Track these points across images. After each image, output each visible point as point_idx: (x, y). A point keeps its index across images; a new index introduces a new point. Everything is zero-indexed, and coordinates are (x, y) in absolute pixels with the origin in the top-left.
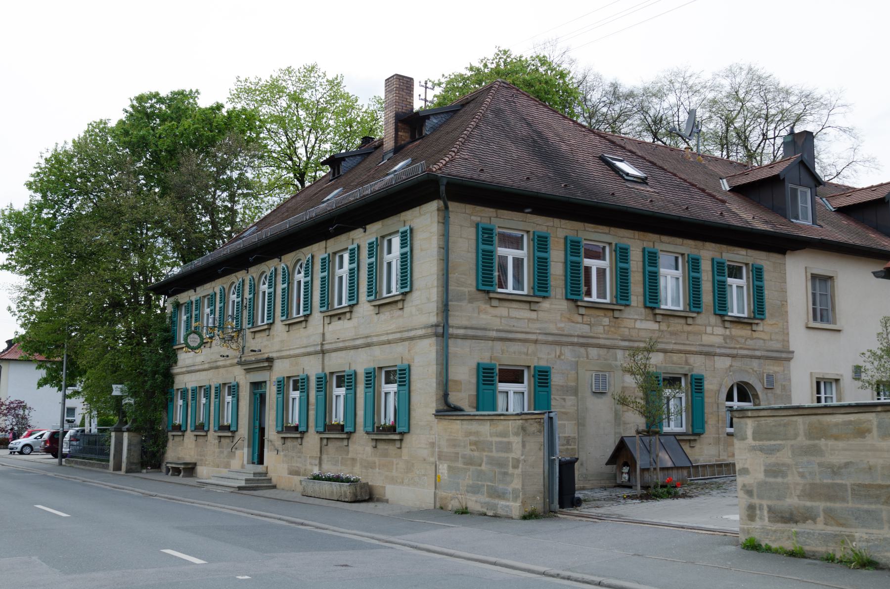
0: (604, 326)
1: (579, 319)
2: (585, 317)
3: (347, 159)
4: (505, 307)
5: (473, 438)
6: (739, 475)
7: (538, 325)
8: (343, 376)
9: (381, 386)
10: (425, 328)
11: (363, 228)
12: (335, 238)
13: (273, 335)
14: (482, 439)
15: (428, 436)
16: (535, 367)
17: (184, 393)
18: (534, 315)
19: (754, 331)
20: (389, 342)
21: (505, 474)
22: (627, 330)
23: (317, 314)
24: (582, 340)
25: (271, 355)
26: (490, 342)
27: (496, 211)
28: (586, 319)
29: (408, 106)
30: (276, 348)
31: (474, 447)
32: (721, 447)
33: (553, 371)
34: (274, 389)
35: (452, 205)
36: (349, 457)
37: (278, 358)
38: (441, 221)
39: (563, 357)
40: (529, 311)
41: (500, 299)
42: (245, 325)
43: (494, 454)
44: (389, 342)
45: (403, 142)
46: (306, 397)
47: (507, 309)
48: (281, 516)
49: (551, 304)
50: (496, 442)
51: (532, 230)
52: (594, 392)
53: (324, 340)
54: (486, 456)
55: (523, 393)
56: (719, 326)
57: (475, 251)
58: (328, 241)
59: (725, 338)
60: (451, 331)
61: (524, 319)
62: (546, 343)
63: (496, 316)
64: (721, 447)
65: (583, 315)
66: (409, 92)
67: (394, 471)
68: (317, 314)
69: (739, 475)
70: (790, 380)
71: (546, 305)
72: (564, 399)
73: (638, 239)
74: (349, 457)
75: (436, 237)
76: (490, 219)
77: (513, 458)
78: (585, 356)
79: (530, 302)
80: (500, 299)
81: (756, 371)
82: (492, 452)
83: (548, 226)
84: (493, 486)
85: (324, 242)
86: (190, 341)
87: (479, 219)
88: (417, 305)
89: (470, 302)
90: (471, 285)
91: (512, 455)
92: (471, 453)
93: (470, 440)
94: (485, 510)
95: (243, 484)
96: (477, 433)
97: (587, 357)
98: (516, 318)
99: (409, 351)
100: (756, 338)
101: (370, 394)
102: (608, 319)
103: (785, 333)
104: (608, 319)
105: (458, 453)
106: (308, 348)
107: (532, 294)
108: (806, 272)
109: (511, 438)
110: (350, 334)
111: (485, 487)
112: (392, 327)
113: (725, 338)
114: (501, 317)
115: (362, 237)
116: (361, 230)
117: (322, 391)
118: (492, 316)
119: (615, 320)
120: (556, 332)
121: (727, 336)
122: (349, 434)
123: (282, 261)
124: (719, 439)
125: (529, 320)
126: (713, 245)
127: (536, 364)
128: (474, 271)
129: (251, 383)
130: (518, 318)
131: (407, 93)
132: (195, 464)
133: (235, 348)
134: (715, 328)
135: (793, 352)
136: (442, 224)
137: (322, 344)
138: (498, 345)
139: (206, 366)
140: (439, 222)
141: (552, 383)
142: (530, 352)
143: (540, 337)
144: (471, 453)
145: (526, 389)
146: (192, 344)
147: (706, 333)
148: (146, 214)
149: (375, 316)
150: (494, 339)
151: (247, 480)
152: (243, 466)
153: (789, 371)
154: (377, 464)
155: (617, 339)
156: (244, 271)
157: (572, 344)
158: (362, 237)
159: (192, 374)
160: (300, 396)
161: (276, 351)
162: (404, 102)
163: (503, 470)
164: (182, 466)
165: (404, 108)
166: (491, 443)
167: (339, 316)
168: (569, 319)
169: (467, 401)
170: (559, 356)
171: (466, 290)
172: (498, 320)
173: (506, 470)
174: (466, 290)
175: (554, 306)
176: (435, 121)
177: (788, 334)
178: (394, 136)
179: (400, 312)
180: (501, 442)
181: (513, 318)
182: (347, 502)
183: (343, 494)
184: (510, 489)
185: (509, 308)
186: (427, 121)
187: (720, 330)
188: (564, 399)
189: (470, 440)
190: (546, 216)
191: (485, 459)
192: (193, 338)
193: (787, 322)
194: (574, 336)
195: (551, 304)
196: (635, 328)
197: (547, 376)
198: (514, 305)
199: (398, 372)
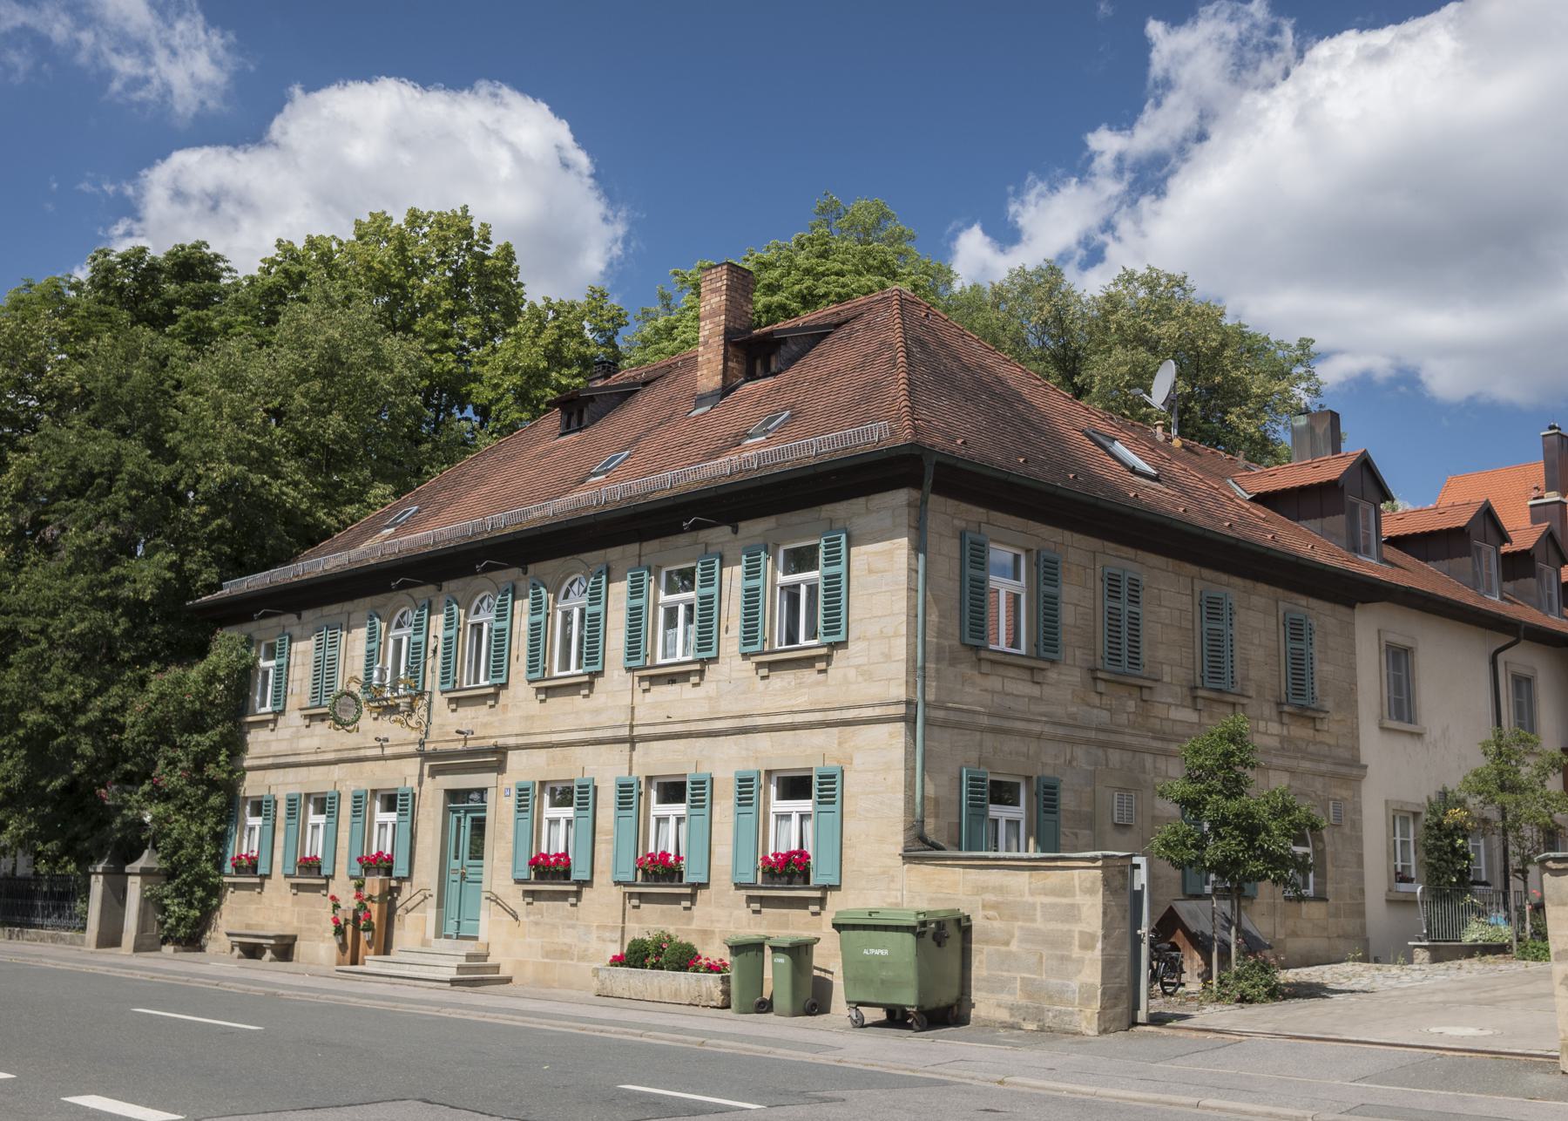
0: (1129, 713)
1: (1096, 700)
2: (1104, 697)
3: (597, 400)
4: (999, 675)
5: (990, 897)
6: (1556, 960)
7: (1043, 708)
12: (662, 540)
13: (505, 706)
14: (1010, 898)
15: (884, 892)
16: (1039, 778)
17: (258, 808)
18: (1035, 691)
19: (1317, 730)
20: (794, 727)
21: (1063, 959)
22: (1157, 721)
23: (616, 673)
24: (1102, 736)
25: (501, 742)
26: (978, 733)
28: (1105, 700)
31: (991, 913)
32: (1278, 920)
33: (1063, 786)
34: (510, 802)
35: (933, 498)
36: (693, 927)
37: (518, 747)
38: (913, 525)
39: (1074, 764)
40: (1030, 684)
41: (993, 662)
43: (1039, 924)
44: (794, 727)
46: (409, 824)
47: (1000, 679)
48: (627, 1030)
49: (1060, 674)
50: (1043, 905)
51: (1035, 548)
52: (1116, 824)
53: (633, 719)
54: (1021, 928)
56: (1275, 721)
57: (958, 578)
58: (645, 544)
59: (1283, 739)
61: (1024, 697)
62: (1053, 739)
63: (986, 690)
64: (1278, 920)
65: (1101, 694)
68: (616, 673)
69: (1556, 960)
70: (1361, 811)
71: (1052, 675)
72: (1076, 835)
73: (1172, 572)
74: (693, 927)
75: (906, 551)
76: (980, 526)
77: (1081, 933)
78: (1104, 762)
79: (1032, 669)
80: (993, 662)
81: (1319, 796)
82: (1033, 920)
83: (1055, 542)
84: (1035, 980)
87: (964, 524)
88: (860, 665)
89: (951, 665)
90: (953, 635)
91: (1077, 928)
93: (983, 900)
94: (1018, 1020)
95: (452, 974)
96: (1001, 890)
97: (1107, 765)
98: (1012, 694)
99: (840, 744)
100: (1321, 742)
102: (1133, 702)
103: (1354, 735)
104: (1133, 702)
106: (597, 732)
107: (1034, 655)
108: (1379, 640)
109: (1077, 898)
110: (702, 710)
111: (1018, 981)
112: (802, 700)
113: (1283, 739)
114: (993, 692)
115: (729, 542)
116: (727, 529)
119: (1142, 704)
120: (1066, 720)
121: (1285, 737)
124: (1274, 906)
125: (1031, 698)
126: (1266, 587)
127: (1040, 774)
128: (958, 612)
129: (446, 790)
130: (1017, 696)
132: (295, 938)
133: (415, 726)
134: (1269, 723)
135: (1366, 767)
136: (914, 530)
138: (989, 739)
140: (910, 526)
141: (1062, 807)
142: (1031, 752)
143: (1047, 729)
145: (1023, 816)
147: (1258, 732)
150: (984, 730)
151: (459, 968)
152: (425, 943)
153: (1360, 797)
155: (1146, 737)
157: (1088, 742)
158: (729, 542)
159: (287, 770)
160: (327, 823)
161: (517, 735)
163: (1058, 953)
165: (738, 321)
166: (1033, 906)
168: (1083, 700)
169: (946, 833)
170: (1070, 762)
172: (989, 696)
173: (1066, 953)
175: (1063, 677)
177: (1358, 737)
180: (1054, 906)
181: (1008, 694)
182: (714, 1007)
183: (704, 993)
184: (1074, 985)
185: (1003, 677)
186: (782, 347)
187: (1274, 728)
188: (1076, 835)
189: (983, 900)
190: (1050, 525)
191: (1017, 933)
192: (345, 704)
193: (1357, 718)
194: (1091, 729)
195: (1060, 674)
196: (1168, 719)
197: (1055, 794)
198: (1011, 672)
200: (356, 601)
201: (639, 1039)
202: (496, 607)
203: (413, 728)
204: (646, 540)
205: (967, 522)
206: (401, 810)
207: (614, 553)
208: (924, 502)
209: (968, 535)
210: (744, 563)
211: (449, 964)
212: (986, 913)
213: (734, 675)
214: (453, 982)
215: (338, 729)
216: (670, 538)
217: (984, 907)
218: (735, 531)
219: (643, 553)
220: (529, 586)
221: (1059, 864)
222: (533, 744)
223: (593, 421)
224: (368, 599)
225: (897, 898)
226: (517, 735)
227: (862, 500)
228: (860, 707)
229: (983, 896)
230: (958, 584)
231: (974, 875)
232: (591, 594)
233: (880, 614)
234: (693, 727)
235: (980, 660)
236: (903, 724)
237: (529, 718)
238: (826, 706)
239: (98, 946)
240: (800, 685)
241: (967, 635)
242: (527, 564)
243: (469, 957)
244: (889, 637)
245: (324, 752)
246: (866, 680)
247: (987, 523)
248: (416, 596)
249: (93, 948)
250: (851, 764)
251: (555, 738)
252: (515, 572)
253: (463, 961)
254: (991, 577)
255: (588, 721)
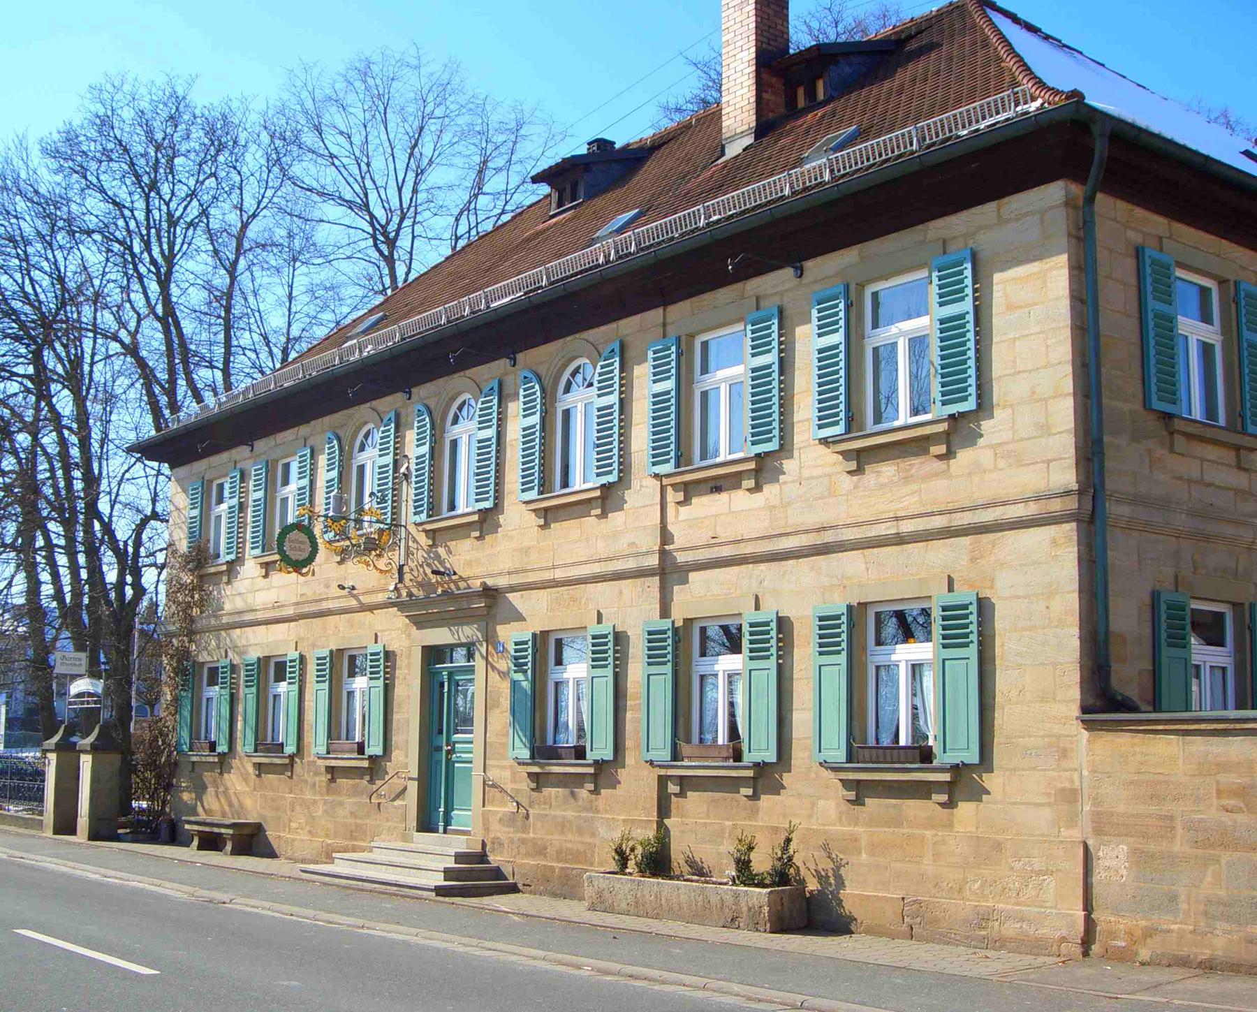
8: (217, 668)
9: (864, 649)
10: (1038, 499)
11: (510, 359)
12: (694, 299)
27: (1169, 224)
29: (779, 39)
30: (506, 563)
31: (1230, 802)
42: (409, 516)
45: (771, 115)
55: (1224, 669)
58: (671, 309)
60: (681, 558)
61: (1230, 489)
63: (1180, 478)
66: (780, 9)
67: (928, 860)
79: (1237, 448)
85: (660, 310)
86: (291, 549)
92: (1226, 819)
95: (439, 880)
101: (377, 689)
105: (1171, 818)
112: (911, 503)
116: (788, 273)
117: (324, 681)
118: (1175, 478)
122: (222, 756)
123: (415, 397)
125: (1237, 491)
129: (423, 647)
131: (776, 12)
137: (663, 554)
139: (290, 611)
140: (1069, 235)
144: (1226, 819)
146: (294, 555)
148: (97, 294)
149: (848, 478)
154: (864, 843)
156: (245, 447)
161: (509, 573)
162: (771, 31)
164: (231, 831)
167: (579, 508)
171: (1126, 407)
174: (1126, 407)
176: (847, 70)
178: (753, 99)
179: (940, 465)
199: (369, 657)
200: (313, 423)
201: (700, 994)
202: (478, 413)
203: (381, 571)
204: (674, 302)
205: (1144, 234)
206: (371, 673)
207: (628, 325)
208: (1090, 200)
209: (1148, 252)
210: (815, 322)
211: (433, 866)
212: (1225, 802)
213: (806, 473)
214: (440, 891)
215: (289, 572)
216: (706, 296)
217: (1219, 792)
218: (800, 273)
219: (668, 321)
220: (519, 381)
221: (1203, 726)
222: (530, 583)
223: (591, 196)
224: (326, 420)
225: (1072, 782)
226: (509, 573)
227: (991, 207)
228: (1004, 504)
229: (1219, 777)
230: (1136, 322)
231: (1198, 745)
232: (599, 389)
233: (1030, 367)
234: (748, 549)
235: (1171, 433)
236: (1074, 525)
237: (526, 551)
238: (950, 506)
239: (56, 832)
240: (907, 479)
241: (1154, 398)
242: (514, 353)
243: (459, 857)
244: (1045, 400)
245: (283, 606)
246: (1010, 465)
247: (1170, 238)
248: (380, 409)
249: (49, 833)
250: (992, 588)
251: (559, 574)
252: (501, 365)
253: (451, 863)
254: (1179, 317)
255: (601, 549)
